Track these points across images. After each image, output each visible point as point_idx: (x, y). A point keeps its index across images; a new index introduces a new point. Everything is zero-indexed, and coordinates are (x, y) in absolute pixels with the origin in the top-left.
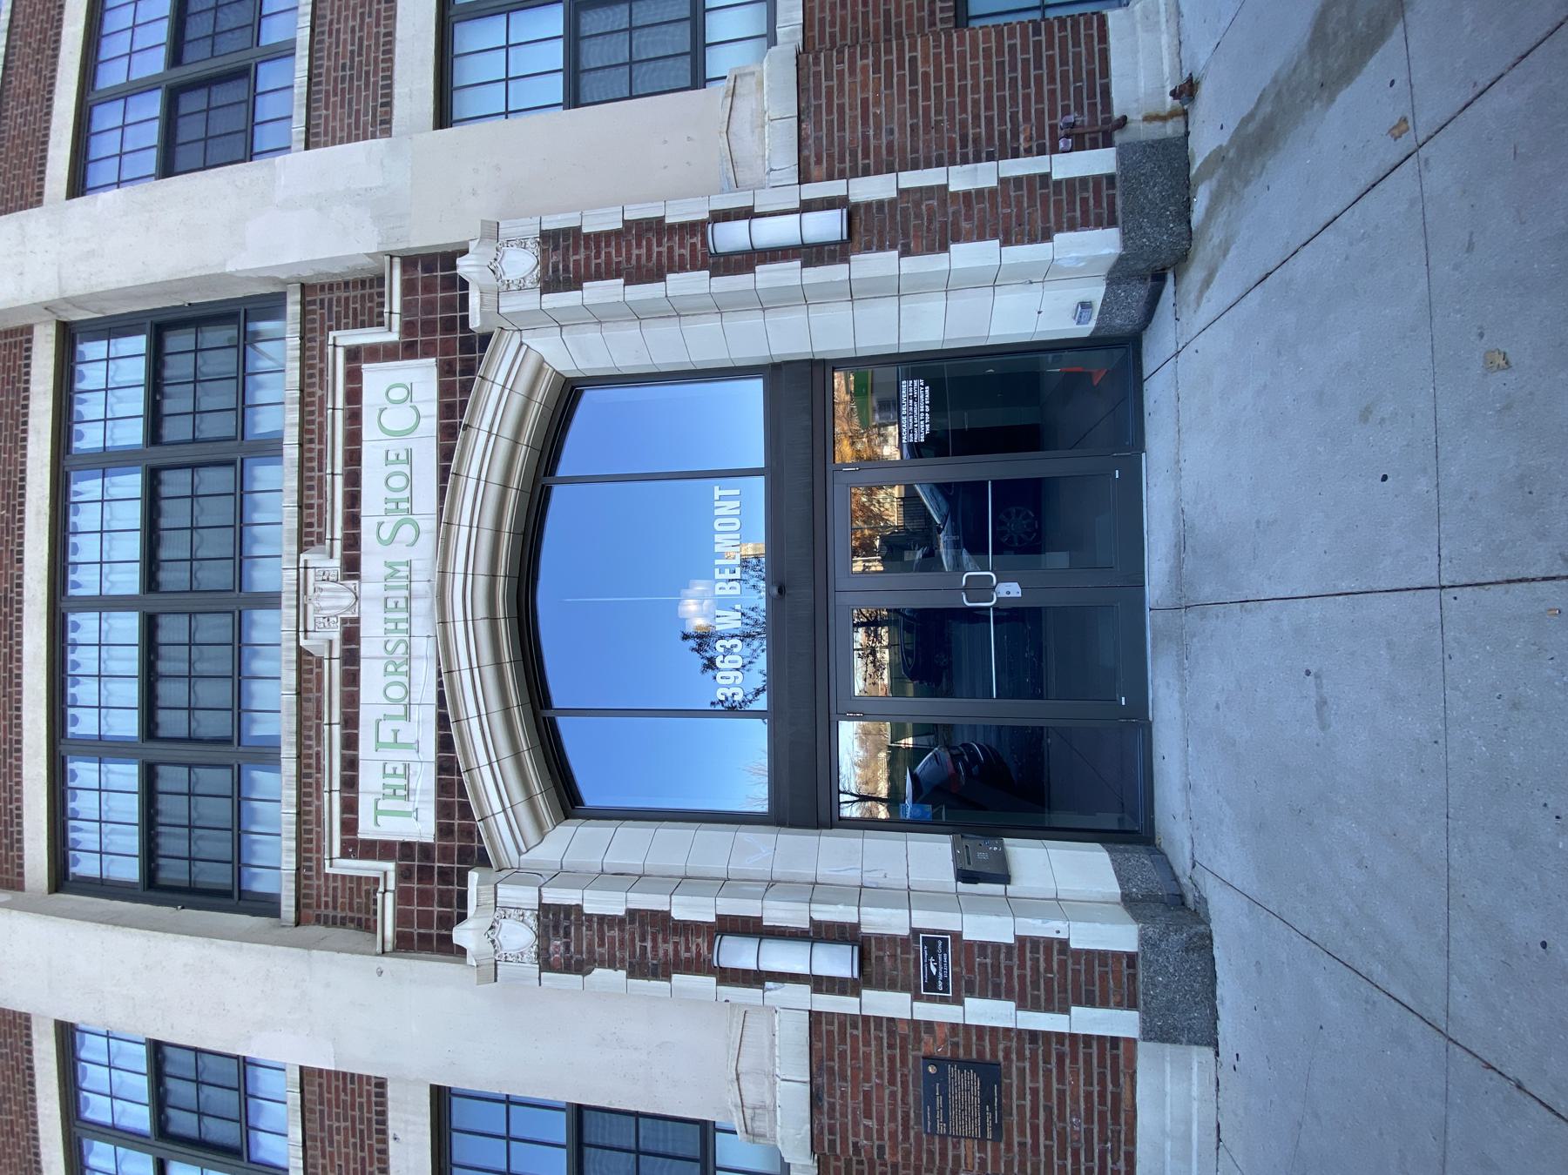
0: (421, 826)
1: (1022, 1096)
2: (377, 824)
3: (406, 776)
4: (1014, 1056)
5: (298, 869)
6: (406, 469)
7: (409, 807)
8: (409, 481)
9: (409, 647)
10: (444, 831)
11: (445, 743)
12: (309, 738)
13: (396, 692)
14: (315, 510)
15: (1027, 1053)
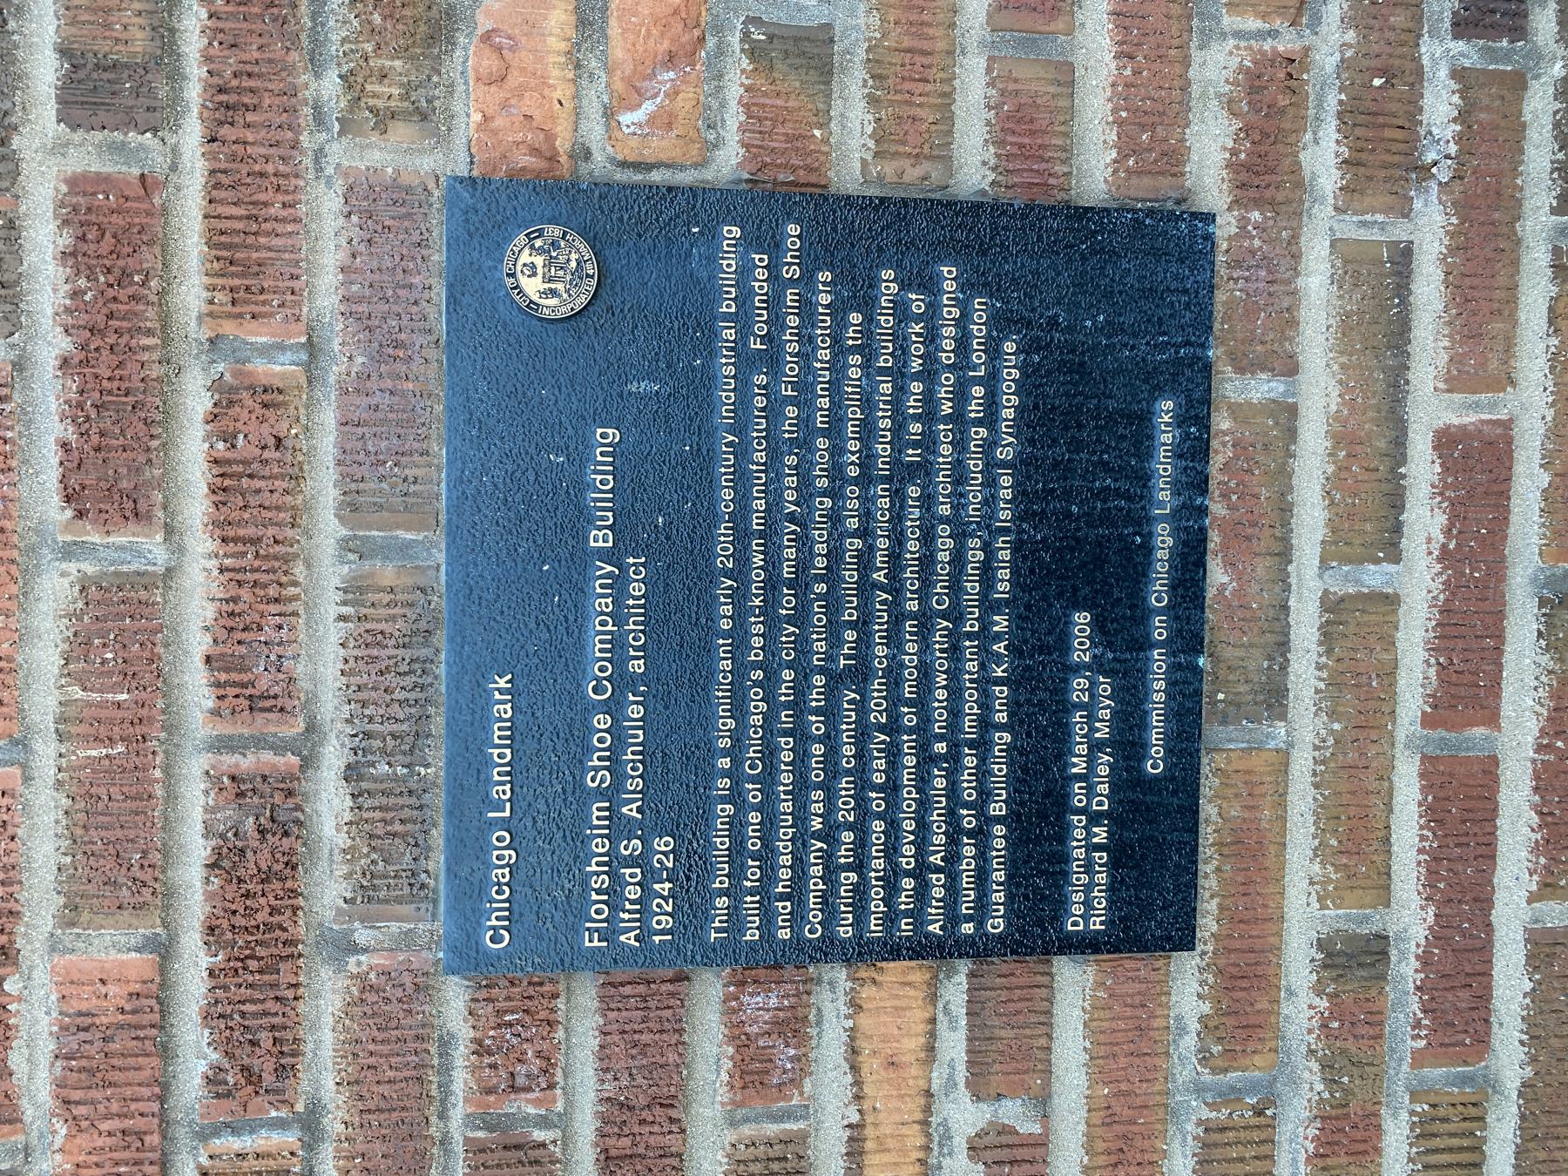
1: (1372, 525)
4: (1322, 156)
15: (1440, 108)
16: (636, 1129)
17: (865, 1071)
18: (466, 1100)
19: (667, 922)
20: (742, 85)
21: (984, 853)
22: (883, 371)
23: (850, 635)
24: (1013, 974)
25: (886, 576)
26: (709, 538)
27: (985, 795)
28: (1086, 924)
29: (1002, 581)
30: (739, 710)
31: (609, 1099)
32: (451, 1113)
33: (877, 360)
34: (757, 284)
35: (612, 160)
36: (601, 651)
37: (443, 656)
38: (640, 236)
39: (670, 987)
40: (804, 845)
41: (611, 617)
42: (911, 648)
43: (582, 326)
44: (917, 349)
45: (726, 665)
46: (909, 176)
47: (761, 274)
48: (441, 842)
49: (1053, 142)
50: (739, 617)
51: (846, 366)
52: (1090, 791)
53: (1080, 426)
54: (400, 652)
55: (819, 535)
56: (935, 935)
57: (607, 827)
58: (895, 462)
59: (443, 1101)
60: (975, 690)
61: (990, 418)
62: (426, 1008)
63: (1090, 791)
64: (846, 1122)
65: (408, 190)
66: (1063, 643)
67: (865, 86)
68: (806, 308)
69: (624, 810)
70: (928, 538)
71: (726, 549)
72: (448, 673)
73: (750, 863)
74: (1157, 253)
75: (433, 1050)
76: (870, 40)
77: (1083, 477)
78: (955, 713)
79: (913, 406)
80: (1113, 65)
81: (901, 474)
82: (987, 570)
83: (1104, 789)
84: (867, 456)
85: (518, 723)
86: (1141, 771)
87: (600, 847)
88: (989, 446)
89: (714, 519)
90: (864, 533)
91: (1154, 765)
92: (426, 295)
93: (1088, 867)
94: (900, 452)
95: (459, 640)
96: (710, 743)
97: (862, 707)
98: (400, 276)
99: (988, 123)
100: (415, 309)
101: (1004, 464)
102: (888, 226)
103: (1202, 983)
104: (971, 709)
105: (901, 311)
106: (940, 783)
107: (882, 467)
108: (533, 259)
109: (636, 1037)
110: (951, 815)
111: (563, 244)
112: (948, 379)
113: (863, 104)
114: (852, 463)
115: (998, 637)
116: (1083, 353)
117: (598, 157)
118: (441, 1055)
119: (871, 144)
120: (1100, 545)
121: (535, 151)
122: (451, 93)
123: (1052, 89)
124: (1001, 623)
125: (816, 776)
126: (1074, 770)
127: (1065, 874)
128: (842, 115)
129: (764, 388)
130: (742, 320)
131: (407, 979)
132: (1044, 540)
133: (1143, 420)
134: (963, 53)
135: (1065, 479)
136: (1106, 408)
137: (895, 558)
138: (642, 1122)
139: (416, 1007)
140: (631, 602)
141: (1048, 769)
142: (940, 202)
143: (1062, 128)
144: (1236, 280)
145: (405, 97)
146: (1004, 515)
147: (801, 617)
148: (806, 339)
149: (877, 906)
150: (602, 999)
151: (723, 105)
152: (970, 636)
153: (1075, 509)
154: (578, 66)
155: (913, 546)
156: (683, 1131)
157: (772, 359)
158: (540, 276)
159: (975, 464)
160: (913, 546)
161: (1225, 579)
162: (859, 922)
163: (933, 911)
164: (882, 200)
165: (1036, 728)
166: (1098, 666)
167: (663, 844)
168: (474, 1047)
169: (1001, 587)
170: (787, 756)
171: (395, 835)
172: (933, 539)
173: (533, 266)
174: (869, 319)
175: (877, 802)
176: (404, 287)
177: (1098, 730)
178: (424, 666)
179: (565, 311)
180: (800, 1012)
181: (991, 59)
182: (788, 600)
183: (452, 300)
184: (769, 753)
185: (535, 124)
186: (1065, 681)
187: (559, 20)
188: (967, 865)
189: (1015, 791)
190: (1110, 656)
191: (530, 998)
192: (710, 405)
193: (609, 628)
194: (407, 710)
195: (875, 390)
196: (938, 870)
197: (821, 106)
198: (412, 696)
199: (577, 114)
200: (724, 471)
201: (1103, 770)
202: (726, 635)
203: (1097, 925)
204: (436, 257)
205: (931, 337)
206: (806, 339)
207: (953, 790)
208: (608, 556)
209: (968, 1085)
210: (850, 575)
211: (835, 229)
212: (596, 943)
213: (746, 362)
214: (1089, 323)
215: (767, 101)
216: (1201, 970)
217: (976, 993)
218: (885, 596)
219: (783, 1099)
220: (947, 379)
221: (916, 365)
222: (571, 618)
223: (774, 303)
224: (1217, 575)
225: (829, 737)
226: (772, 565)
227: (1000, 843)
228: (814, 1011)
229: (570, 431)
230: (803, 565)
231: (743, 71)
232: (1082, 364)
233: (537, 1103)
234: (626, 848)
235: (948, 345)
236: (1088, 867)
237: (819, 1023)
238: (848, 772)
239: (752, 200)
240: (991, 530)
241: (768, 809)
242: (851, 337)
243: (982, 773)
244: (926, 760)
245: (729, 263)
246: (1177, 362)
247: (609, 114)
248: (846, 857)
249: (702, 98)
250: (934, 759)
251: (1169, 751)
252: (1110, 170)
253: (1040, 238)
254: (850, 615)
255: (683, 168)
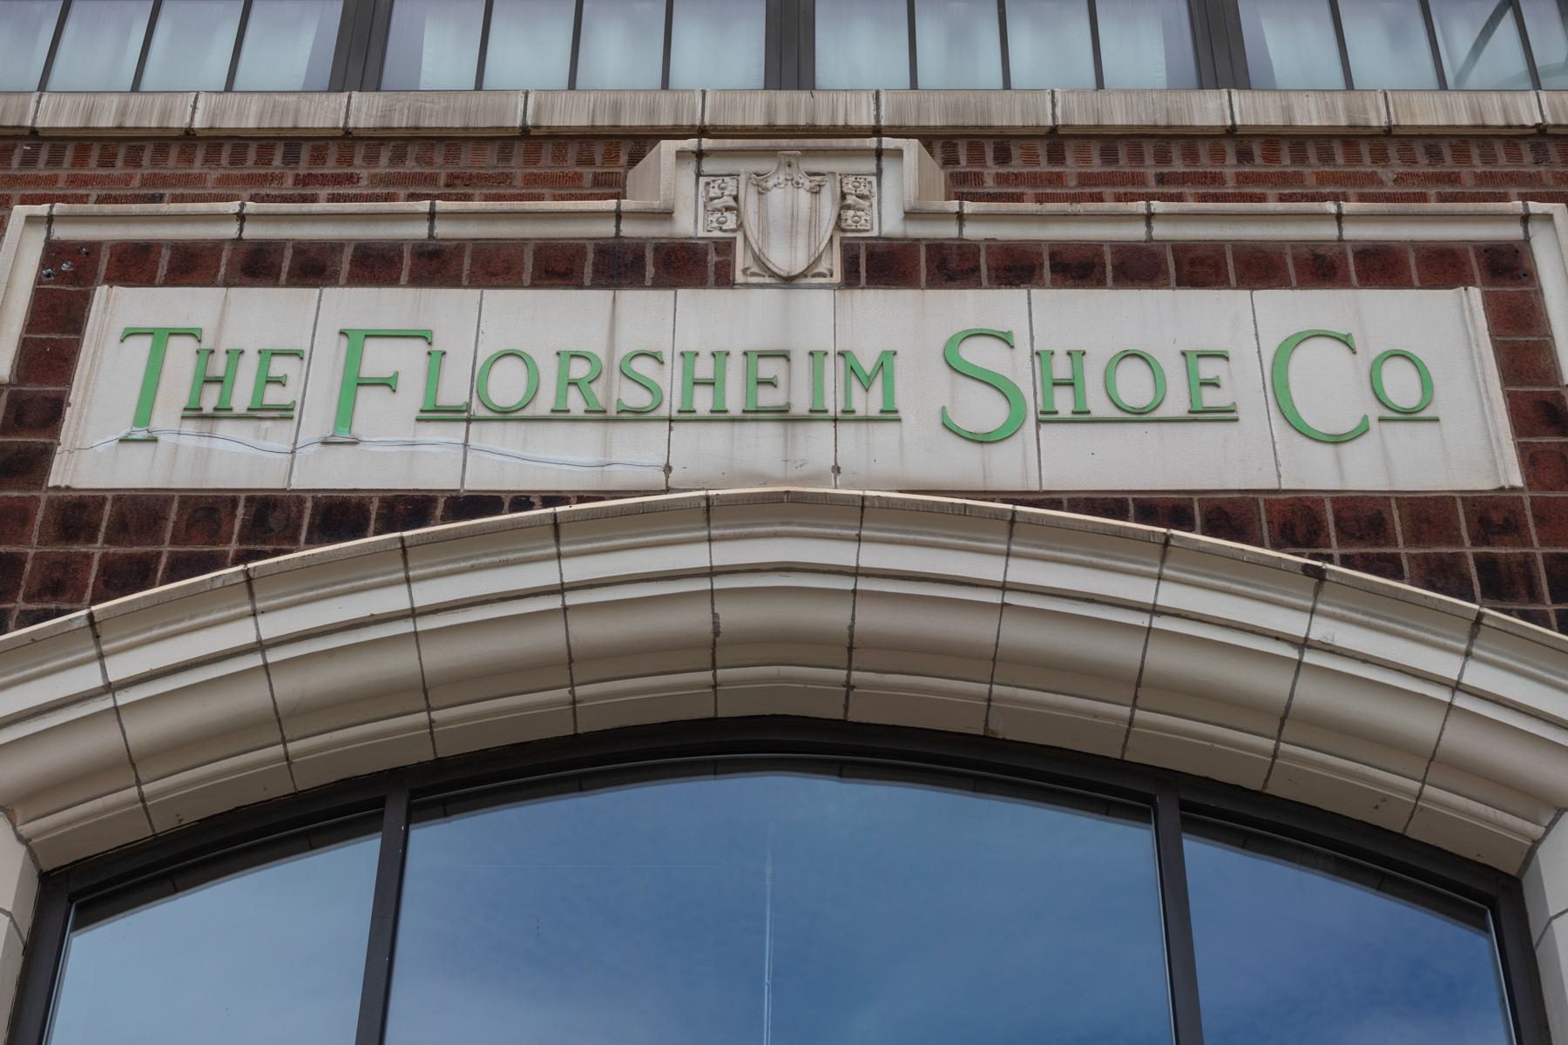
0: (102, 447)
2: (131, 333)
3: (258, 413)
5: (34, 132)
6: (1177, 404)
7: (166, 417)
8: (1139, 416)
9: (638, 416)
10: (78, 513)
11: (340, 515)
12: (398, 158)
13: (507, 386)
14: (1044, 167)
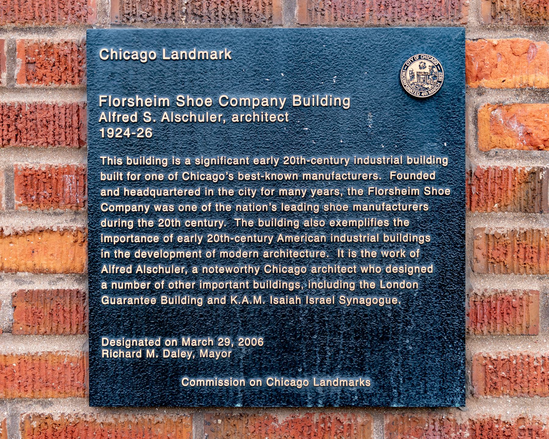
16: (5, 123)
17: (31, 238)
18: (23, 41)
19: (111, 135)
20: (517, 168)
21: (142, 293)
22: (381, 237)
23: (251, 223)
24: (78, 312)
25: (281, 241)
26: (299, 152)
27: (171, 293)
28: (105, 347)
29: (279, 300)
30: (214, 168)
31: (21, 109)
32: (16, 33)
33: (387, 234)
34: (421, 174)
35: (478, 106)
36: (243, 101)
37: (239, 28)
38: (441, 118)
39: (76, 138)
40: (147, 202)
41: (261, 105)
42: (245, 254)
43: (398, 91)
44: (393, 254)
45: (236, 162)
46: (476, 252)
47: (426, 176)
48: (149, 28)
49: (498, 325)
50: (260, 167)
51: (383, 219)
52: (173, 348)
53: (356, 338)
54: (241, 8)
55: (300, 207)
56: (101, 269)
57: (157, 106)
58: (337, 244)
59: (22, 30)
60: (223, 290)
61: (359, 292)
62: (69, 21)
63: (173, 348)
64: (4, 228)
65: (459, 11)
66: (247, 333)
67: (520, 229)
68: (412, 198)
69: (165, 113)
70: (300, 261)
71: (293, 161)
72: (232, 30)
73: (139, 175)
74: (443, 376)
75: (47, 25)
76: (543, 230)
77: (331, 341)
78: (211, 277)
79: (365, 252)
80: (538, 356)
81: (330, 246)
82: (284, 292)
83: (174, 355)
84: (340, 231)
85: (207, 62)
86: (183, 374)
87: (148, 101)
88: (346, 291)
89: (307, 154)
90: (302, 230)
91: (187, 382)
92: (410, 19)
93: (134, 348)
94: (342, 247)
95: (248, 34)
96: (197, 154)
97: (216, 229)
98: (419, 7)
99: (505, 292)
100: (403, 14)
101: (337, 299)
102: (451, 239)
103: (70, 416)
104: (215, 285)
105: (412, 245)
106: (177, 270)
107: (335, 237)
108: (428, 67)
109: (52, 123)
110: (161, 276)
111: (435, 81)
112: (377, 269)
113: (512, 228)
114: (336, 223)
115: (251, 299)
116: (393, 339)
117: (479, 99)
118: (45, 28)
119: (492, 232)
120: (298, 351)
121: (480, 69)
122: (506, 30)
123: (524, 324)
124: (258, 300)
125: (181, 207)
126: (183, 339)
127: (131, 337)
128: (506, 218)
129: (372, 179)
130: (404, 167)
131: (83, 12)
132: (299, 321)
133: (361, 372)
134: (540, 278)
135: (330, 332)
136: (365, 352)
137: (289, 245)
138: (9, 126)
139: (70, 16)
140: (266, 115)
141: (185, 326)
142: (464, 264)
143: (505, 330)
144: (434, 424)
145: (503, 9)
146: (312, 299)
147: (260, 198)
148: (396, 198)
149: (116, 239)
150: (71, 105)
151: (507, 159)
152: (251, 284)
153: (315, 337)
154: (522, 89)
155: (296, 254)
156: (3, 146)
157: (385, 182)
158: (420, 71)
159: (337, 284)
160: (296, 254)
161: (280, 422)
162: (108, 230)
163: (113, 268)
164: (464, 236)
165: (205, 320)
166: (236, 350)
167: (149, 132)
168: (49, 44)
169: (276, 299)
170: (191, 192)
171: (153, 6)
172: (300, 265)
173: (425, 67)
174: (406, 230)
175: (168, 238)
176: (414, 9)
177: (204, 351)
178: (234, 19)
179: (404, 82)
180: (62, 203)
181: (537, 292)
182: (268, 191)
183: (407, 32)
184: (192, 184)
185: (494, 69)
186: (229, 335)
187: (543, 80)
188: (136, 285)
189: (173, 310)
190: (241, 358)
191: (72, 70)
192: (362, 153)
193: (254, 105)
194: (213, 12)
195: (372, 233)
196: (134, 270)
197: (509, 207)
198: (220, 14)
199: (499, 89)
200: (331, 159)
201: (183, 354)
202: (251, 161)
203: (105, 353)
204: (428, 23)
205: (399, 261)
206: (396, 198)
207: (173, 277)
208: (288, 104)
209: (21, 291)
210: (281, 222)
211: (448, 212)
212: (101, 101)
213: (384, 168)
214: (408, 341)
215: (510, 180)
216: (77, 415)
217: (68, 294)
218: (271, 241)
219: (18, 196)
220: (378, 269)
221: (385, 253)
222: (258, 87)
223: (412, 182)
224: (282, 418)
225: (200, 214)
226: (285, 183)
227: (147, 301)
228: (61, 211)
229: (348, 86)
230: (286, 199)
231: (524, 168)
232: (388, 339)
233: (20, 74)
234: (147, 114)
235: (395, 269)
236: (134, 348)
237: (55, 214)
238: (183, 224)
239: (461, 172)
240: (304, 293)
241: (166, 183)
242: (398, 221)
243: (182, 291)
244: (189, 263)
245: (430, 160)
246: (390, 389)
247: (500, 105)
248: (141, 223)
249: (510, 149)
250: (189, 267)
251: (193, 389)
252: (486, 355)
253: (448, 315)
254: (261, 223)
255: (476, 139)
